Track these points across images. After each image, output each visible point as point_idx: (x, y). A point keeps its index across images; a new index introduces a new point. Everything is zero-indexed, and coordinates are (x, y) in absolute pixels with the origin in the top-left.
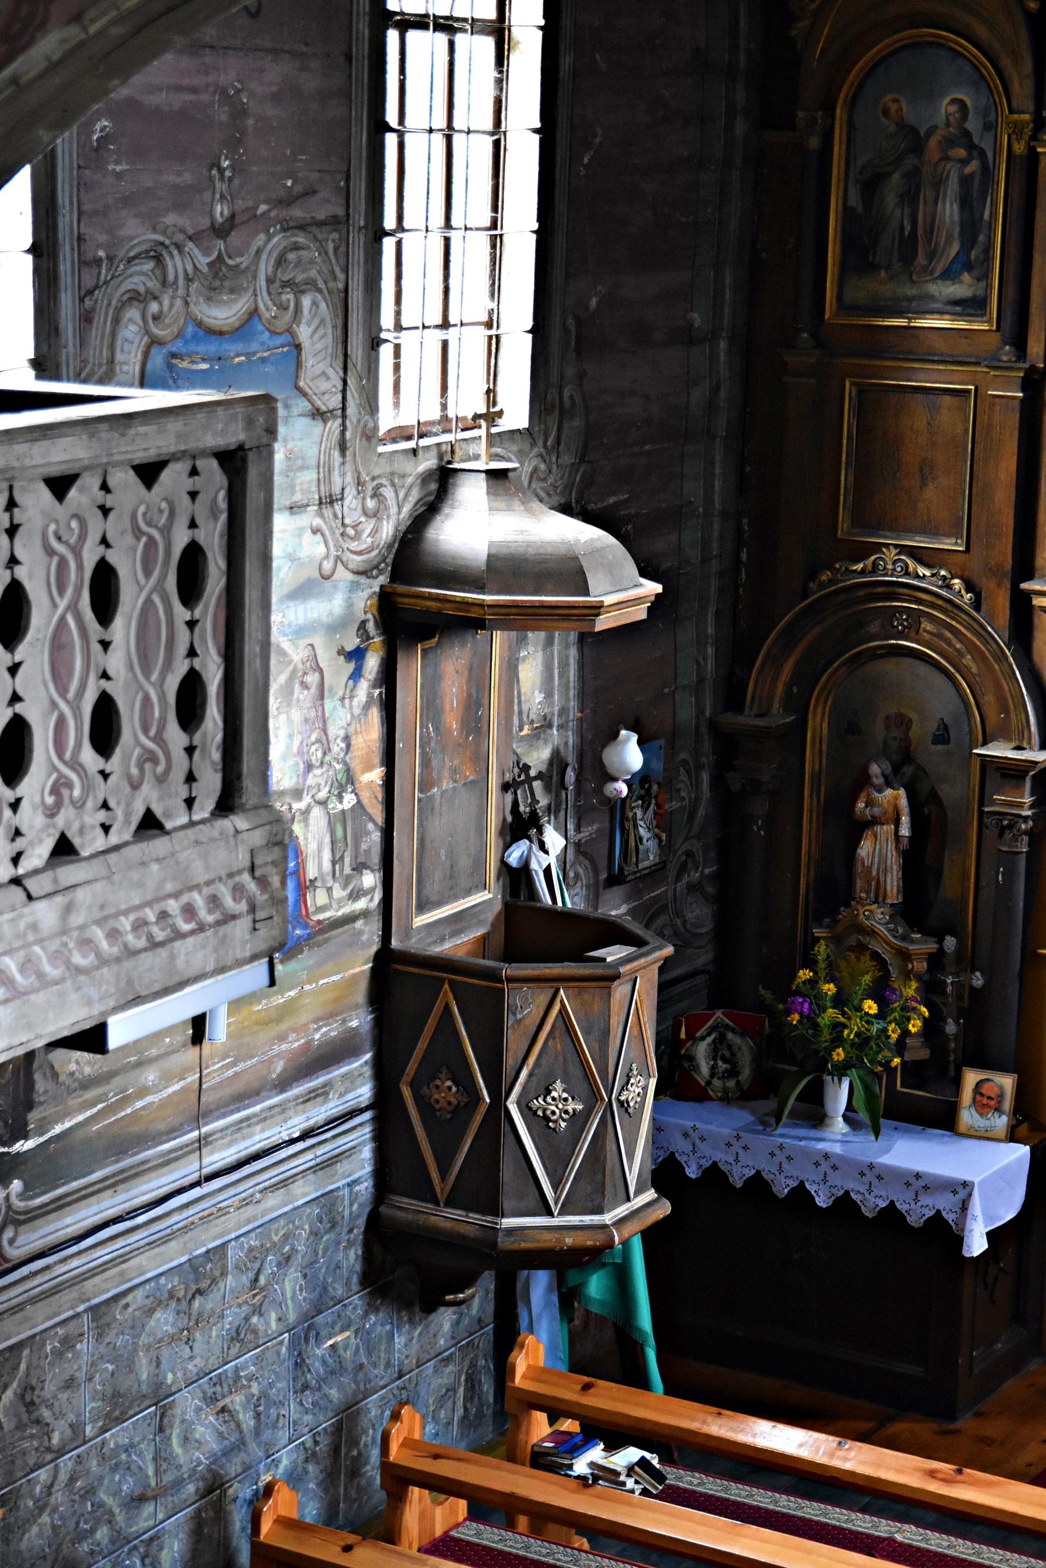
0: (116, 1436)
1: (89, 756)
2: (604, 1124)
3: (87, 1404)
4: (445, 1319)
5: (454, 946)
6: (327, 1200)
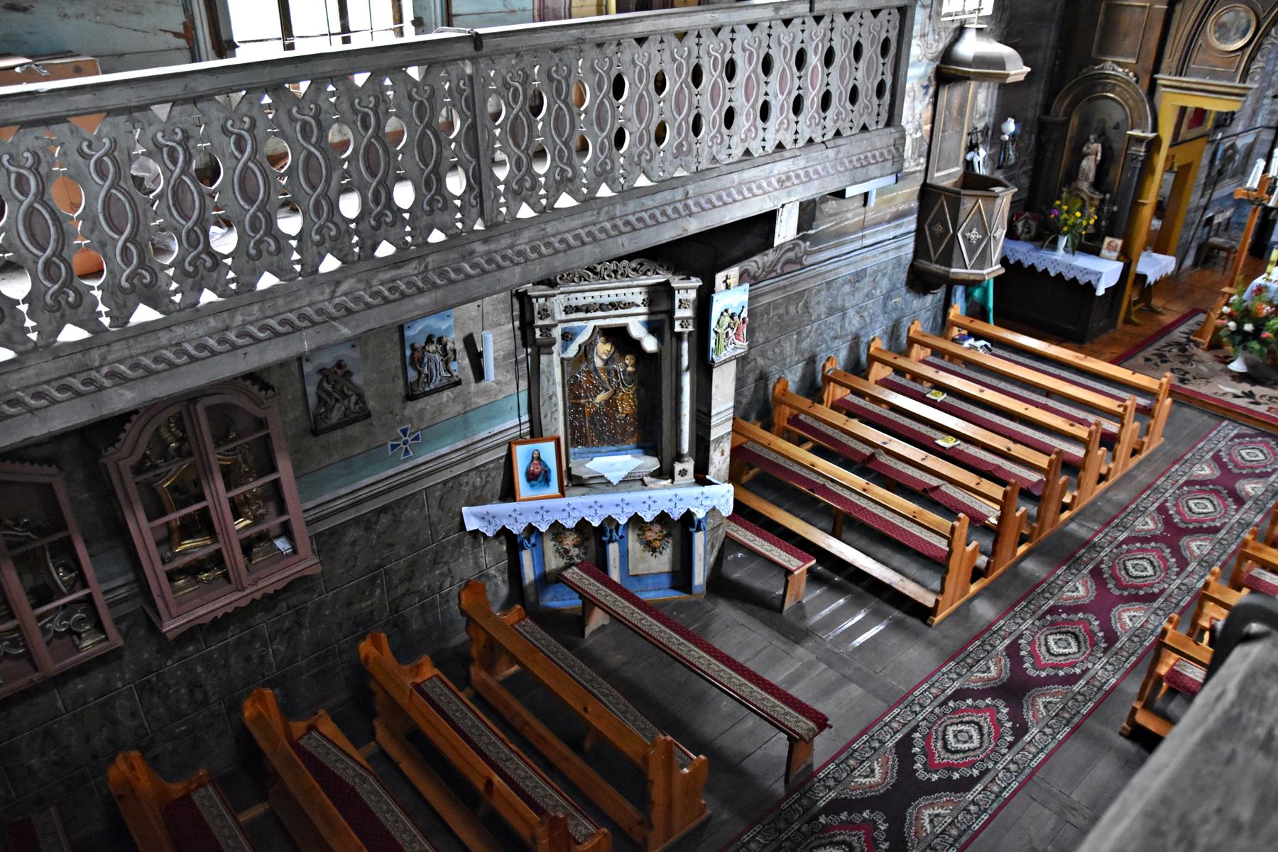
0: (830, 319)
1: (848, 105)
2: (988, 242)
3: (822, 309)
4: (929, 298)
5: (947, 183)
6: (898, 259)
